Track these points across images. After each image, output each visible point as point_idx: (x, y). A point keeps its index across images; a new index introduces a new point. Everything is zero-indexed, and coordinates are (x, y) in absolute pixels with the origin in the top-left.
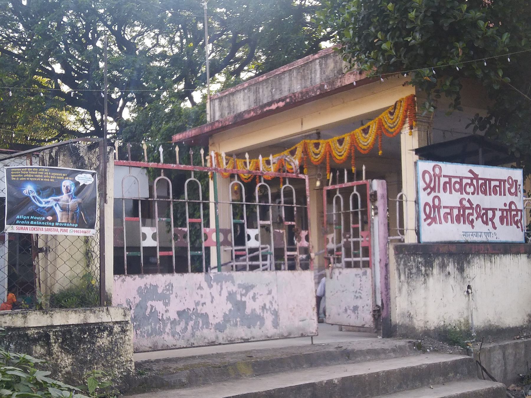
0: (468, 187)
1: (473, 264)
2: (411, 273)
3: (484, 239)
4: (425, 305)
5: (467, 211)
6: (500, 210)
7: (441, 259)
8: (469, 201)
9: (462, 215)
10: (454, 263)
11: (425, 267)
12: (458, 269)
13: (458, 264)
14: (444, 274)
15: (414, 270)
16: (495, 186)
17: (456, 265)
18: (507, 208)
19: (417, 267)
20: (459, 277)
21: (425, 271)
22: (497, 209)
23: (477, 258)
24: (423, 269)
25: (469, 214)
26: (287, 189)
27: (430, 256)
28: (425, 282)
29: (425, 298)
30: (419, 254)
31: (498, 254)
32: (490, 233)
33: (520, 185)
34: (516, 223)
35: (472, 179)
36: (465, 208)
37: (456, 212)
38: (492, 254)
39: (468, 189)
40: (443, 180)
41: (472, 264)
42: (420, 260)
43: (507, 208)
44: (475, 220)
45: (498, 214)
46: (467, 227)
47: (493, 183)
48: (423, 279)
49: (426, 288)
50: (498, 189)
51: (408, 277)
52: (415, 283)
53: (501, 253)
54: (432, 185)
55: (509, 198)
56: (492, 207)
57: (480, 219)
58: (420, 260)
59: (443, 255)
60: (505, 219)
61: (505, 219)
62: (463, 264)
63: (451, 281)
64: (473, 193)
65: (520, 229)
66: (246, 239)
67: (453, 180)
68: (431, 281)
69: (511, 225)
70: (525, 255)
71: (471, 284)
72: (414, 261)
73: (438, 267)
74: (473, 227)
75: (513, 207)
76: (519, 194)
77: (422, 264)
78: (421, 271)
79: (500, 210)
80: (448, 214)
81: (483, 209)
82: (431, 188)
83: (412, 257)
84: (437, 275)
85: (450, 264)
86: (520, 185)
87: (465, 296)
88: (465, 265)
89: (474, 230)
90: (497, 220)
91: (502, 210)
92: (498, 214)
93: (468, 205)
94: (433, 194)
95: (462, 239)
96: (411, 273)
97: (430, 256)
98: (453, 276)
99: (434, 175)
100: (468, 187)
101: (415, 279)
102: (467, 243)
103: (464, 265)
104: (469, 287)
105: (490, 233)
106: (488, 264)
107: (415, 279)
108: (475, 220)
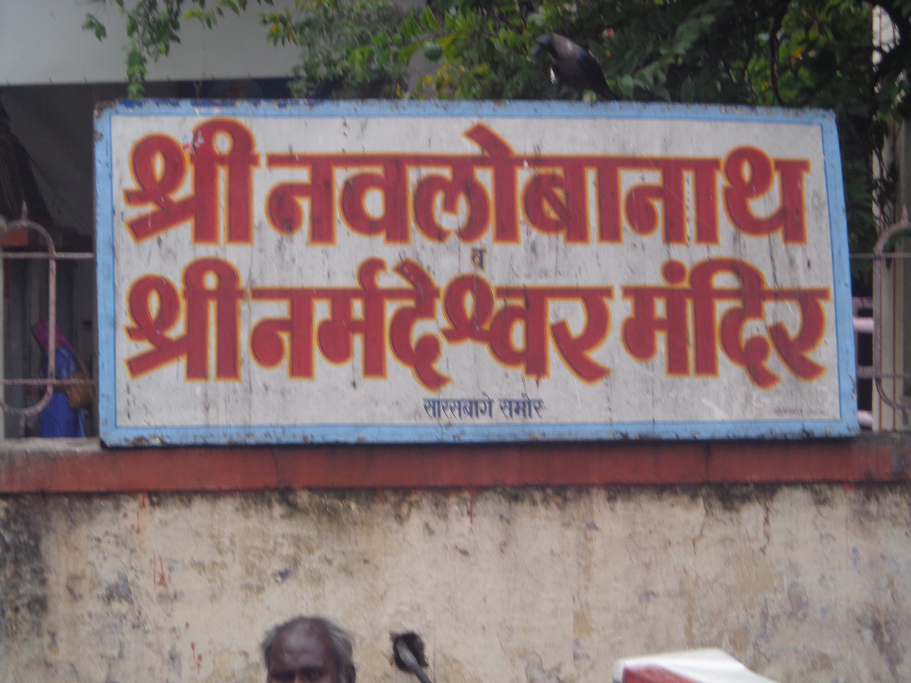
16: (641, 194)
47: (629, 180)
80: (280, 324)
81: (505, 292)
92: (620, 310)
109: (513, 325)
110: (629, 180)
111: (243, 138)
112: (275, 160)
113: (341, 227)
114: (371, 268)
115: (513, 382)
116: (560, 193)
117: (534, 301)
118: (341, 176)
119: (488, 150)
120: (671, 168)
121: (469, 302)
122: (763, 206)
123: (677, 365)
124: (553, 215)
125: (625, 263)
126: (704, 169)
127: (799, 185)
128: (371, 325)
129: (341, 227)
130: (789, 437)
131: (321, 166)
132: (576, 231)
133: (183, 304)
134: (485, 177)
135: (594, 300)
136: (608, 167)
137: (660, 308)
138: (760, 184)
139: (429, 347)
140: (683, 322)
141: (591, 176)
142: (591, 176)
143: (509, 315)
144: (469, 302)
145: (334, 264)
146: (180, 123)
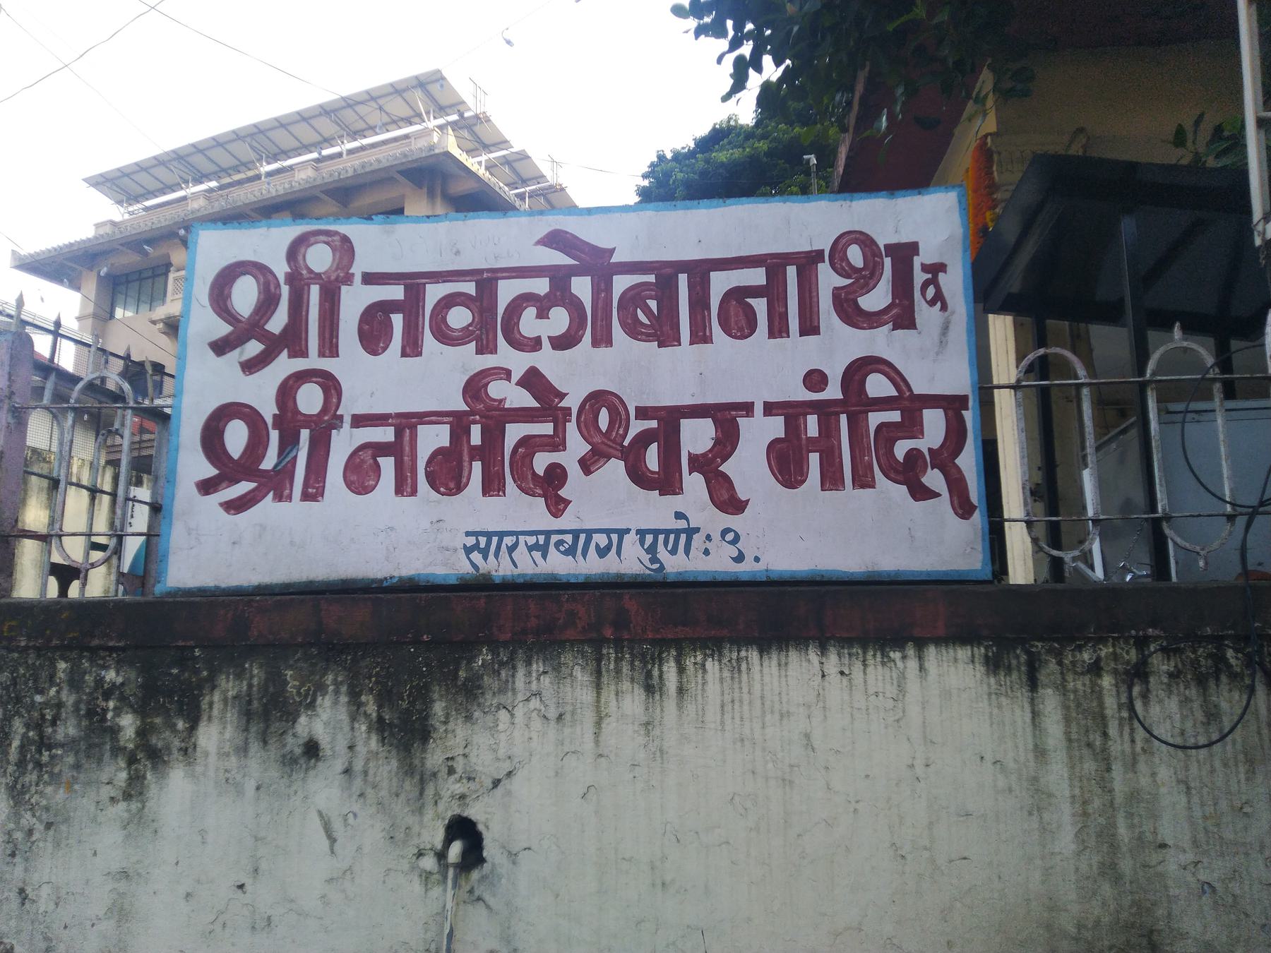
0: (530, 313)
1: (507, 699)
2: (44, 743)
3: (631, 561)
4: (120, 912)
5: (514, 433)
6: (770, 409)
7: (257, 673)
8: (532, 380)
9: (478, 446)
10: (354, 695)
11: (142, 710)
12: (380, 726)
13: (384, 698)
14: (274, 750)
15: (69, 729)
16: (738, 295)
17: (371, 708)
18: (833, 392)
19: (91, 713)
20: (386, 769)
21: (142, 733)
22: (747, 408)
23: (537, 667)
24: (128, 723)
25: (529, 445)
26: (920, 462)
27: (184, 660)
28: (134, 790)
29: (125, 874)
30: (111, 650)
31: (713, 644)
32: (691, 532)
33: (936, 269)
34: (908, 474)
35: (560, 278)
36: (497, 418)
37: (433, 438)
38: (662, 644)
39: (529, 324)
40: (355, 301)
41: (490, 700)
42: (111, 676)
43: (833, 392)
44: (574, 470)
45: (759, 432)
46: (519, 510)
47: (720, 283)
48: (123, 775)
49: (140, 823)
50: (760, 306)
51: (21, 764)
52: (61, 794)
53: (741, 641)
54: (277, 322)
55: (838, 346)
56: (711, 400)
57: (615, 469)
58: (111, 676)
59: (274, 651)
60: (814, 458)
61: (814, 458)
62: (422, 696)
63: (324, 789)
64: (563, 342)
65: (944, 503)
66: (1260, 568)
67: (434, 293)
68: (175, 790)
69: (863, 480)
70: (963, 653)
71: (474, 812)
72: (75, 682)
73: (232, 715)
74: (557, 506)
75: (877, 386)
76: (926, 314)
77: (123, 698)
78: (115, 731)
79: (770, 409)
80: (380, 449)
81: (643, 413)
82: (265, 337)
83: (62, 665)
84: (223, 755)
85: (324, 702)
86: (936, 269)
87: (426, 876)
88: (438, 708)
89: (568, 521)
90: (748, 465)
91: (791, 412)
92: (759, 432)
93: (521, 398)
94: (284, 365)
95: (458, 567)
96: (44, 743)
97: (184, 660)
98: (339, 765)
99: (292, 278)
100: (530, 313)
101: (67, 774)
102: (479, 586)
103: (428, 703)
104: (464, 830)
105: (691, 532)
106: (632, 701)
107: (67, 774)
108: (574, 470)
109: (651, 447)
110: (720, 283)
111: (345, 248)
112: (371, 279)
113: (429, 341)
114: (475, 387)
115: (655, 510)
116: (653, 304)
117: (669, 420)
118: (434, 293)
119: (425, 716)
120: (774, 264)
121: (604, 419)
122: (876, 299)
123: (831, 479)
124: (646, 321)
125: (765, 368)
126: (808, 262)
127: (224, 485)
128: (489, 451)
129: (429, 341)
130: (236, 224)
131: (414, 283)
132: (664, 334)
133: (274, 435)
134: (582, 287)
135: (727, 419)
136: (700, 271)
137: (812, 425)
138: (865, 278)
139: (556, 475)
140: (835, 435)
141: (791, 271)
142: (791, 271)
143: (644, 439)
144: (604, 419)
145: (428, 379)
146: (269, 245)
